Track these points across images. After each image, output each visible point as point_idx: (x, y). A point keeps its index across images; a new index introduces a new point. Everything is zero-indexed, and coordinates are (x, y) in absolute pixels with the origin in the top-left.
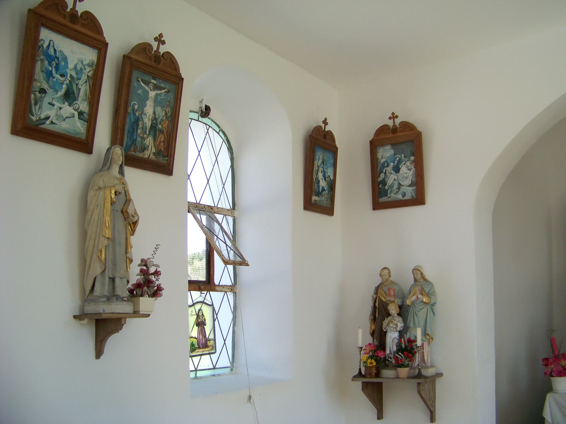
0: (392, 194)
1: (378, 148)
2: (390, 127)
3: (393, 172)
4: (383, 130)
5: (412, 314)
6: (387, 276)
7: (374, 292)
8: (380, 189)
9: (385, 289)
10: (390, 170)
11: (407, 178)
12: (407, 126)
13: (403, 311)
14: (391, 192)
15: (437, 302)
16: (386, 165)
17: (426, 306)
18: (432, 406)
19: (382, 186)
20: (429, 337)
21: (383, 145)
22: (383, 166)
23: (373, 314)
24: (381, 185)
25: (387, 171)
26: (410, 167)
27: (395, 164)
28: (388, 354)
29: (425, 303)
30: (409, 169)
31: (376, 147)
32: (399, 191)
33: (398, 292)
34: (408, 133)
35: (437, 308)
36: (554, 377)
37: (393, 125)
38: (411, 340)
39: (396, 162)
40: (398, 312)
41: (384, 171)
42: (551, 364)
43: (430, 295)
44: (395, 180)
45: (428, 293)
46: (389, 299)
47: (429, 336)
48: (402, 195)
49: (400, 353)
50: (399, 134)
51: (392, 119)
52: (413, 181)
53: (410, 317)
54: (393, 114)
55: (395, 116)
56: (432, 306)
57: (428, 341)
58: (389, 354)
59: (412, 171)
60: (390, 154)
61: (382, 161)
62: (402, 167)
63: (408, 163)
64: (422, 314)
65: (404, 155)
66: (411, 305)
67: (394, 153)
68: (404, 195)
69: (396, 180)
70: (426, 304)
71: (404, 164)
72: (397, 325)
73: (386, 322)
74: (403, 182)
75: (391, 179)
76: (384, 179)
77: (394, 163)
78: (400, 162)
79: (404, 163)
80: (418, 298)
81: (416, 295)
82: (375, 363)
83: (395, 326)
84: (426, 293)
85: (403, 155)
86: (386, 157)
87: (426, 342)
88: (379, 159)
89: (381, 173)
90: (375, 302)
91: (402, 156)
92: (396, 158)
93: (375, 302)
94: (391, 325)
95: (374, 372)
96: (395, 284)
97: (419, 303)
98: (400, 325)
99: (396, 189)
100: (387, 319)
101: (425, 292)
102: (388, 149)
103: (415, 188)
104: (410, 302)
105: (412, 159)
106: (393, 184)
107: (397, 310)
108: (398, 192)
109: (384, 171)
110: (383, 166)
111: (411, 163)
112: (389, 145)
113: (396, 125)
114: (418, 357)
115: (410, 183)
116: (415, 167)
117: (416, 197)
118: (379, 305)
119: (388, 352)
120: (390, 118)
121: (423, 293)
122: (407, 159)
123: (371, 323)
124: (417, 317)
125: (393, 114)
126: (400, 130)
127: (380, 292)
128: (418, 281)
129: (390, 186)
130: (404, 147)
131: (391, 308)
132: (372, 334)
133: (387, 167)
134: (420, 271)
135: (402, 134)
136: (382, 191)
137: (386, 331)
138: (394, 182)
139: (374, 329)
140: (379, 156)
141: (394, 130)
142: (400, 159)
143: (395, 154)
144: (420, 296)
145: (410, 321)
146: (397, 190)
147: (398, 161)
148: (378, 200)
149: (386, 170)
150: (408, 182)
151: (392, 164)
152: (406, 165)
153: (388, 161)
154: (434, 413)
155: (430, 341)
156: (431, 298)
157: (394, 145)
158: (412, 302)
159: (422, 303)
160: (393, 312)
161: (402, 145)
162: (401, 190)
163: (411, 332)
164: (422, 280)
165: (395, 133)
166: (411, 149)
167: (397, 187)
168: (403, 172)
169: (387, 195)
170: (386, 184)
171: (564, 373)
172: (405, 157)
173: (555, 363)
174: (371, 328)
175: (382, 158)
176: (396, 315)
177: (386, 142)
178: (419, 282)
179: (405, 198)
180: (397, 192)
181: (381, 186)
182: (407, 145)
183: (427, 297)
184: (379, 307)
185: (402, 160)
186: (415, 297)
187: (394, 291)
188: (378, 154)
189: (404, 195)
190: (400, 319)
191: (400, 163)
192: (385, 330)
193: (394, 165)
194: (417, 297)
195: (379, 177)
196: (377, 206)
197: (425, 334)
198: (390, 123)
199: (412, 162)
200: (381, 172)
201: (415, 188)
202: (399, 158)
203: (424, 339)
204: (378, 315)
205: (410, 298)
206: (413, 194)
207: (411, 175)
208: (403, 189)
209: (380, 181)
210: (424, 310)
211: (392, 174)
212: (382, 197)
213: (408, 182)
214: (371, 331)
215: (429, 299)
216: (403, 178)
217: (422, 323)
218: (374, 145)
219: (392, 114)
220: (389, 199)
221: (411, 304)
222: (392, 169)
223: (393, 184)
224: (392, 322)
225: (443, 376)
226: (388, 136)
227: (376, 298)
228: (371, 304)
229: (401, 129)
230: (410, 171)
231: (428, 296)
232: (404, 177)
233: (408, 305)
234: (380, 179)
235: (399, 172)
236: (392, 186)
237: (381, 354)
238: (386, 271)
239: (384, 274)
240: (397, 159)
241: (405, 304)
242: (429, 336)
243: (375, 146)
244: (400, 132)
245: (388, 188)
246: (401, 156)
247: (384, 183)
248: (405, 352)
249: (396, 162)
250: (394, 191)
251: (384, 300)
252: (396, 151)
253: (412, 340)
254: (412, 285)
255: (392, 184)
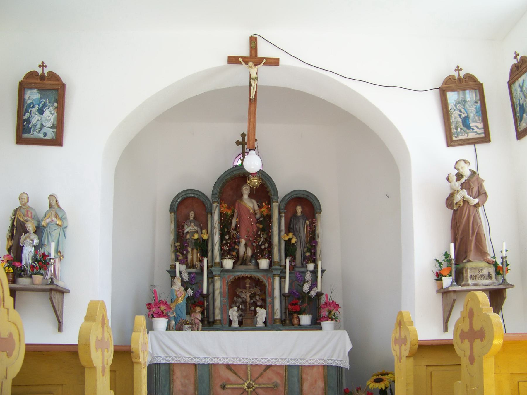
0: (35, 133)
1: (26, 90)
2: (39, 74)
3: (37, 113)
4: (32, 75)
5: (47, 234)
6: (26, 201)
7: (13, 214)
8: (24, 126)
9: (23, 211)
10: (35, 111)
11: (49, 120)
12: (53, 76)
13: (39, 230)
14: (34, 131)
15: (68, 227)
16: (32, 106)
17: (59, 228)
18: (61, 317)
19: (26, 124)
20: (60, 255)
21: (31, 88)
22: (29, 106)
23: (10, 232)
24: (25, 123)
25: (32, 111)
26: (53, 112)
27: (40, 107)
28: (24, 265)
29: (58, 225)
30: (51, 114)
31: (24, 88)
32: (41, 130)
33: (35, 216)
34: (54, 82)
35: (68, 231)
36: (155, 318)
37: (42, 73)
38: (45, 255)
39: (41, 105)
40: (35, 231)
41: (30, 111)
42: (153, 307)
43: (63, 220)
44: (38, 120)
45: (61, 218)
46: (27, 219)
47: (61, 254)
48: (43, 135)
49: (36, 262)
50: (46, 82)
51: (42, 68)
52: (54, 124)
53: (45, 235)
54: (43, 63)
55: (44, 65)
56: (65, 229)
57: (59, 258)
58: (25, 264)
59: (54, 115)
60: (36, 98)
61: (29, 102)
62: (46, 110)
63: (51, 108)
64: (55, 233)
65: (49, 100)
66: (46, 226)
67: (40, 97)
68: (45, 135)
69: (39, 121)
70: (59, 227)
71: (48, 108)
72: (33, 240)
73: (23, 237)
74: (45, 123)
75: (35, 119)
76: (29, 118)
77: (39, 105)
78: (44, 105)
79: (48, 107)
80: (52, 220)
81: (51, 217)
82: (12, 271)
83: (31, 242)
84: (59, 217)
85: (47, 100)
86: (32, 99)
87: (58, 259)
88: (26, 99)
89: (26, 113)
90: (13, 222)
91: (47, 101)
92: (41, 102)
93: (13, 222)
94: (28, 240)
95: (11, 280)
96: (32, 209)
97: (53, 225)
98: (36, 241)
99: (39, 129)
100: (24, 235)
101: (58, 216)
102: (35, 93)
103: (55, 130)
104: (45, 223)
105: (55, 106)
106: (36, 124)
107: (34, 228)
108: (41, 132)
109: (30, 111)
110: (29, 106)
111: (55, 109)
112: (36, 90)
113: (44, 74)
114: (51, 269)
115: (52, 125)
116: (57, 113)
117: (56, 138)
118: (17, 224)
119: (24, 263)
120: (40, 66)
121: (57, 217)
122: (50, 104)
123: (8, 239)
124: (51, 235)
125: (43, 63)
126: (47, 79)
127: (18, 213)
128: (53, 207)
129: (34, 125)
130: (49, 93)
131: (29, 226)
132: (9, 250)
133: (33, 108)
134: (55, 198)
135: (49, 82)
136: (25, 128)
137: (23, 246)
138: (37, 122)
139: (11, 246)
140: (27, 97)
141: (42, 77)
142: (44, 104)
143: (41, 98)
144: (54, 219)
145: (45, 237)
146: (40, 130)
147: (42, 105)
148: (22, 135)
149: (31, 111)
150: (50, 124)
151: (37, 106)
152: (49, 109)
153: (34, 103)
154: (61, 323)
155: (61, 258)
156: (64, 222)
157: (41, 90)
158: (47, 223)
159: (55, 225)
160: (31, 229)
161: (48, 92)
162: (42, 130)
163: (45, 249)
164: (56, 207)
165: (43, 80)
166: (55, 97)
167: (40, 127)
168: (46, 115)
169: (30, 133)
170: (30, 123)
171: (162, 315)
172: (49, 102)
173: (156, 306)
174: (8, 245)
175: (29, 99)
176: (32, 232)
177: (34, 86)
178: (54, 208)
179: (46, 138)
180: (39, 131)
181: (25, 123)
182: (52, 92)
183: (60, 220)
184: (17, 226)
185: (46, 104)
186: (50, 220)
187: (31, 213)
188: (25, 95)
189: (45, 135)
190: (36, 236)
191: (45, 107)
192: (22, 245)
193: (39, 107)
194: (52, 219)
195: (25, 115)
196: (20, 140)
197: (58, 251)
198: (40, 71)
199: (55, 107)
200: (27, 111)
201: (55, 130)
202: (44, 102)
203: (57, 256)
204: (16, 233)
205: (46, 219)
206: (53, 135)
207: (53, 119)
208: (45, 130)
209: (25, 119)
210: (58, 231)
211: (36, 115)
212: (26, 134)
213: (50, 124)
214: (8, 247)
215: (62, 222)
216: (46, 120)
217: (56, 240)
218: (23, 87)
219: (42, 63)
220: (32, 136)
221: (47, 225)
222: (37, 110)
223: (36, 124)
224: (29, 238)
225: (70, 293)
226: (36, 81)
227: (14, 218)
228: (9, 224)
229: (48, 77)
230: (53, 115)
231: (61, 220)
232: (47, 120)
233: (43, 226)
234: (25, 117)
235: (43, 114)
236: (35, 125)
237: (17, 264)
238: (25, 195)
239: (23, 198)
240: (42, 103)
241: (40, 225)
242: (61, 254)
243: (24, 87)
244: (47, 80)
245: (32, 127)
246: (46, 101)
247: (28, 121)
248: (40, 262)
249: (41, 105)
250: (37, 130)
251: (22, 220)
252: (42, 96)
253: (46, 255)
254: (48, 211)
255: (36, 123)
